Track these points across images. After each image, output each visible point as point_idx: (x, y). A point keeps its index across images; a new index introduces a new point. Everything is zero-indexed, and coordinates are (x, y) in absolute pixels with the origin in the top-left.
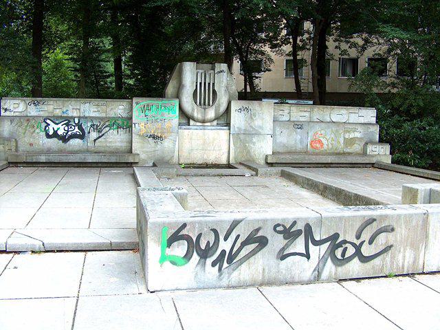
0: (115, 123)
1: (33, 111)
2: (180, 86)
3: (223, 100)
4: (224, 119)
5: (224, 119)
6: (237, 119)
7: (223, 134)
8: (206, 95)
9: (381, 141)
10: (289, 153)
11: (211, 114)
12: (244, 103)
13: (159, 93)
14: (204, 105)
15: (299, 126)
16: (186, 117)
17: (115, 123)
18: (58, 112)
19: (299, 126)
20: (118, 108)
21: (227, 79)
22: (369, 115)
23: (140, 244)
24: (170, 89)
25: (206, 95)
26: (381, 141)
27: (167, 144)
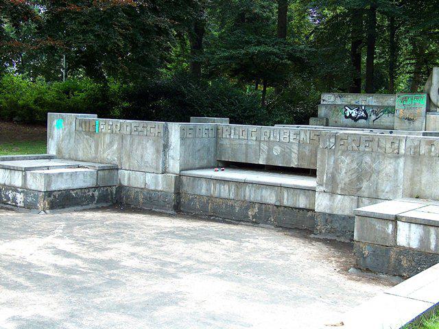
1: (339, 102)
2: (431, 85)
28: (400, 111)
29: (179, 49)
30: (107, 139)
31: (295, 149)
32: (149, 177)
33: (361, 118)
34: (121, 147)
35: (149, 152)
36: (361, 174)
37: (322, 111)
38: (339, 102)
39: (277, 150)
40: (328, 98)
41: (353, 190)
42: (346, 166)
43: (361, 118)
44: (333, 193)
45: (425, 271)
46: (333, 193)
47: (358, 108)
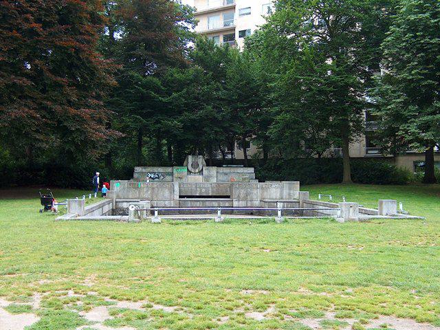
0: (168, 174)
1: (144, 170)
2: (188, 162)
3: (201, 167)
4: (201, 172)
5: (201, 172)
6: (205, 172)
7: (201, 177)
8: (195, 165)
9: (256, 178)
10: (374, 194)
11: (197, 171)
12: (207, 167)
13: (182, 165)
14: (195, 168)
15: (226, 174)
16: (189, 172)
17: (168, 174)
18: (151, 171)
19: (226, 174)
20: (169, 170)
21: (201, 160)
22: (252, 170)
23: (226, 34)
24: (185, 163)
25: (195, 165)
26: (256, 178)
27: (184, 180)
28: (176, 174)
29: (300, 50)
30: (145, 190)
31: (210, 189)
32: (167, 202)
33: (156, 178)
34: (153, 192)
35: (167, 193)
36: (247, 195)
37: (135, 175)
38: (144, 170)
39: (203, 190)
40: (138, 169)
41: (245, 199)
42: (243, 192)
43: (156, 178)
44: (239, 200)
45: (391, 206)
46: (239, 200)
47: (154, 173)
